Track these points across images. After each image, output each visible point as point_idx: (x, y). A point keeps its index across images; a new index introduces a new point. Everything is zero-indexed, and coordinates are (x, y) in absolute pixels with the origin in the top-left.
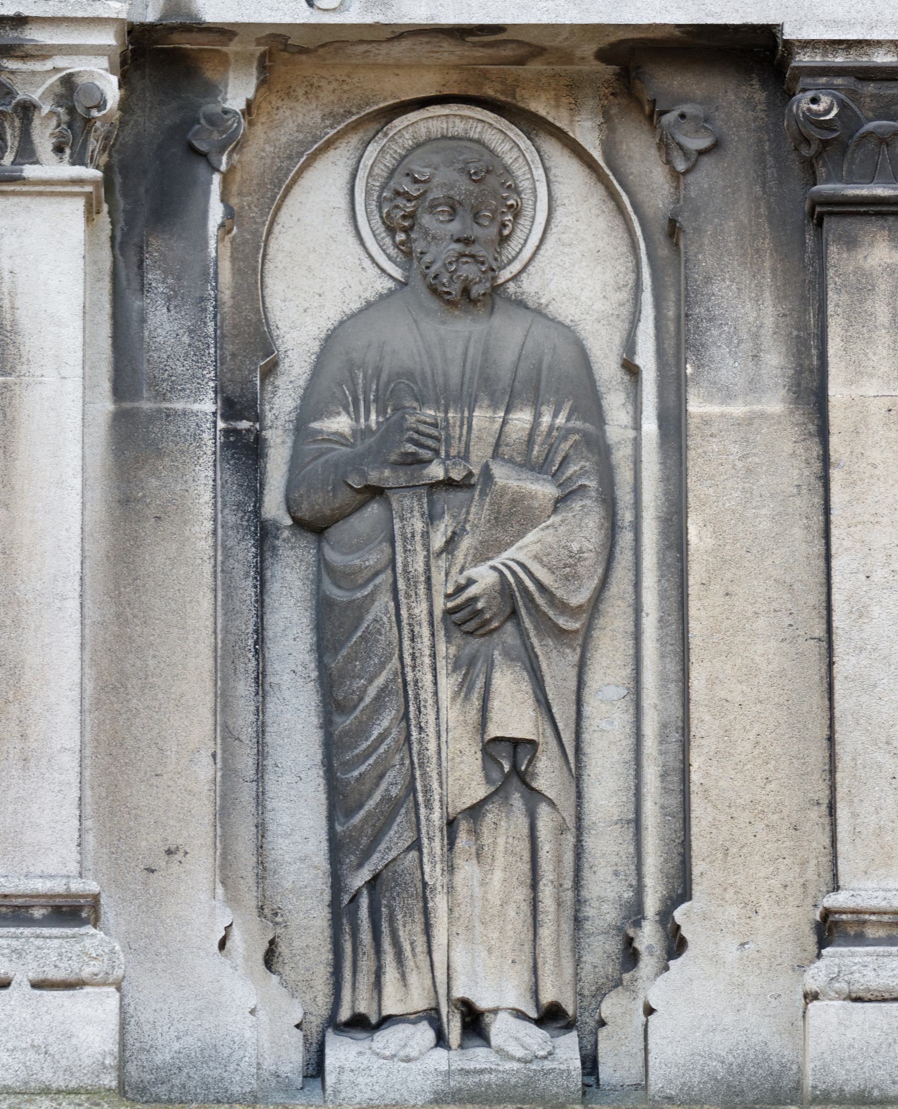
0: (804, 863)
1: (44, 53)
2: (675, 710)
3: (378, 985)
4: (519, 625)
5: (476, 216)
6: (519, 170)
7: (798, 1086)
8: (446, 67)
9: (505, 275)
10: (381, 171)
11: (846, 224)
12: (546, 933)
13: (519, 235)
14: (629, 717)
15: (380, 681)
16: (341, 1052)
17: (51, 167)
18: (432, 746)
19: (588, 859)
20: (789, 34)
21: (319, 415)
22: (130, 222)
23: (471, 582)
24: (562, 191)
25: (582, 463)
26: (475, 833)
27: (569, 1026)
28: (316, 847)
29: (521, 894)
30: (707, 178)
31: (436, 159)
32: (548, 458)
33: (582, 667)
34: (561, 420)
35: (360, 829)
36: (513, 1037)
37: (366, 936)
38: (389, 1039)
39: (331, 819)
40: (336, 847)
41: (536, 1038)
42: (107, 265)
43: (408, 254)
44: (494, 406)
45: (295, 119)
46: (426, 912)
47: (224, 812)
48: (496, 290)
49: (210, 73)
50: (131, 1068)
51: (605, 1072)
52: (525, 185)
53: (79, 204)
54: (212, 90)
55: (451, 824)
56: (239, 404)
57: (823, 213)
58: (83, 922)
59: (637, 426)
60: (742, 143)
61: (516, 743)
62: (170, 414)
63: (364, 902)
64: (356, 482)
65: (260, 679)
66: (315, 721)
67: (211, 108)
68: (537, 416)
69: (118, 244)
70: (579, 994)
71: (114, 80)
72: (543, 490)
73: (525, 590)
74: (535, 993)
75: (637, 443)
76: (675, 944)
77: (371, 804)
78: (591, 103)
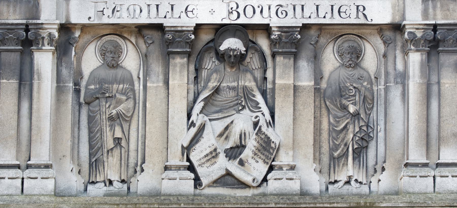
0: (163, 158)
1: (46, 29)
2: (144, 133)
3: (96, 176)
4: (120, 119)
5: (115, 53)
6: (122, 46)
7: (161, 193)
8: (111, 29)
9: (119, 62)
10: (100, 46)
11: (173, 55)
12: (123, 168)
13: (122, 56)
14: (137, 134)
15: (98, 128)
16: (90, 187)
17: (47, 47)
18: (105, 139)
19: (130, 156)
20: (165, 25)
21: (89, 86)
22: (60, 54)
23: (112, 113)
24: (129, 49)
25: (130, 93)
26: (112, 152)
27: (126, 183)
28: (87, 155)
29: (119, 162)
30: (152, 47)
31: (109, 44)
32: (125, 93)
33: (130, 126)
34: (127, 86)
35: (94, 152)
36: (117, 185)
37: (94, 169)
38: (97, 185)
39: (89, 150)
40: (90, 155)
41: (120, 184)
42: (56, 62)
43: (104, 59)
44: (117, 84)
45: (87, 37)
46: (104, 165)
47: (72, 149)
48: (118, 65)
49: (73, 31)
50: (57, 190)
51: (131, 190)
52: (123, 48)
53: (51, 53)
54: (73, 33)
55: (108, 151)
56: (77, 84)
57: (169, 53)
58: (49, 168)
59: (140, 87)
60: (157, 42)
61: (119, 138)
62: (65, 86)
63: (94, 163)
64: (94, 97)
65: (79, 128)
66: (87, 134)
67: (73, 36)
68: (124, 86)
69: (58, 59)
70: (127, 178)
71: (57, 33)
72: (124, 98)
73: (121, 114)
74: (121, 178)
75: (139, 89)
76: (142, 170)
77: (96, 148)
78: (134, 35)
